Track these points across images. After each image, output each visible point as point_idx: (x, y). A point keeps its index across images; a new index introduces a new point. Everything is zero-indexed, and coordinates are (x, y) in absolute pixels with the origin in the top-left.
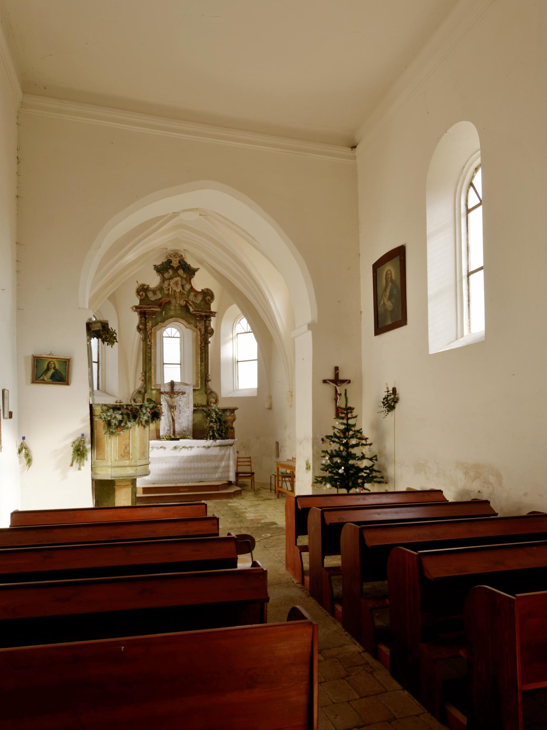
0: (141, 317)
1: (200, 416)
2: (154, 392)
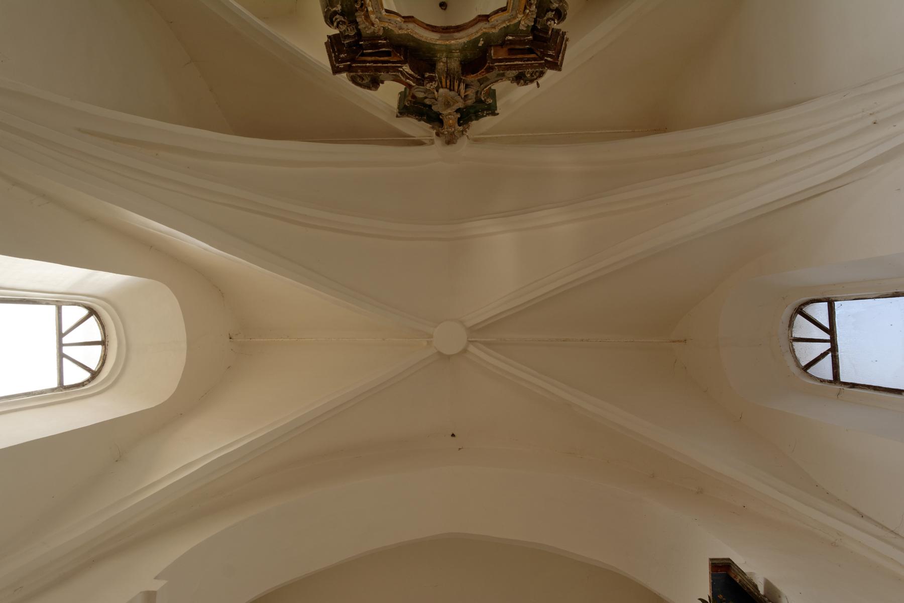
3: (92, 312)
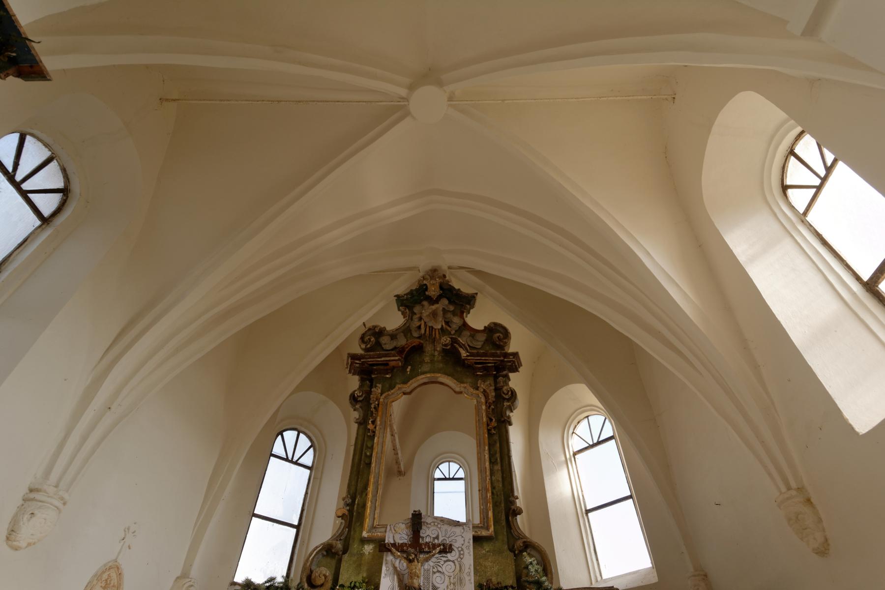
0: (362, 380)
2: (368, 549)
3: (785, 188)
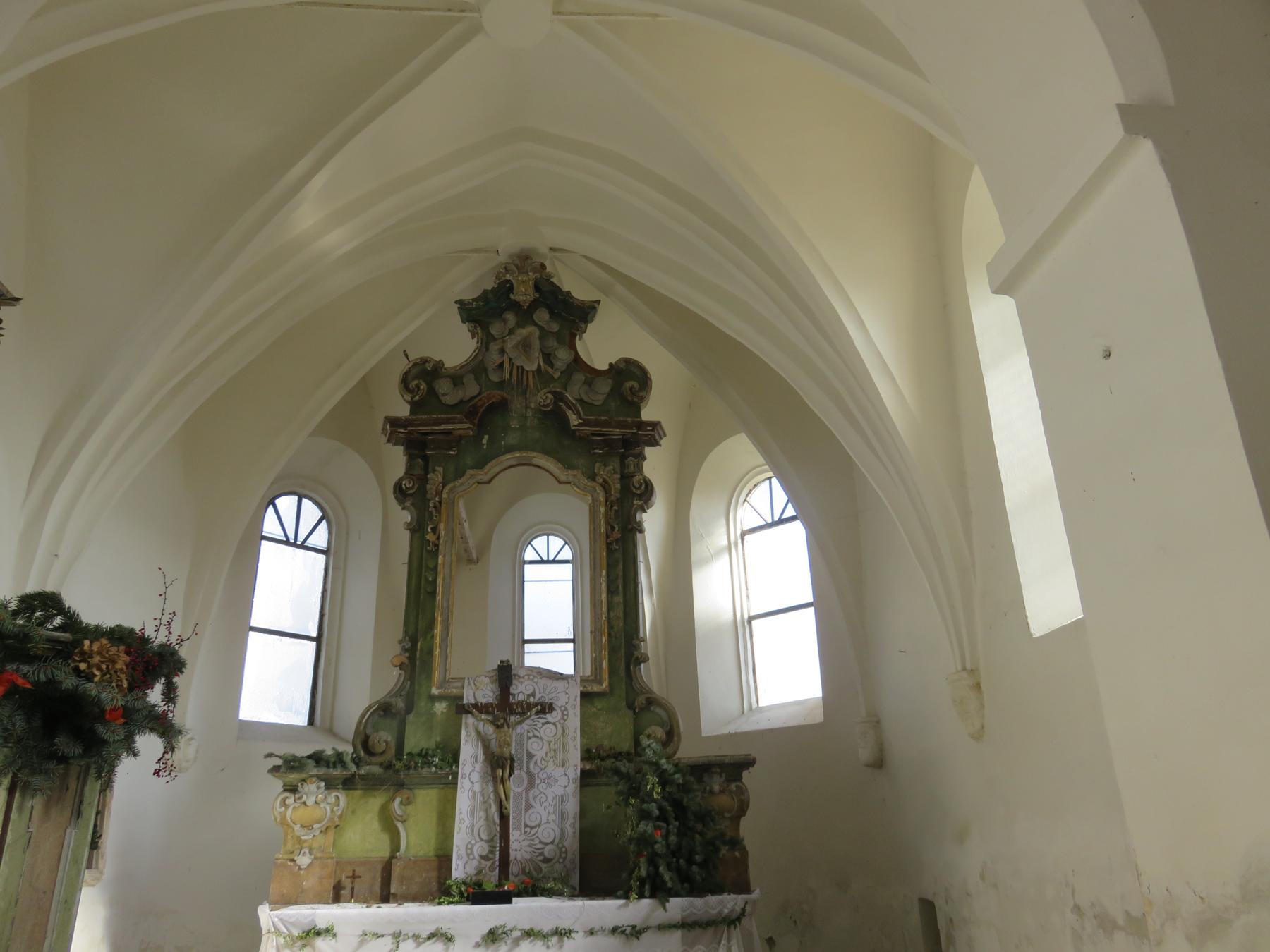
0: (411, 458)
1: (608, 794)
2: (440, 707)
